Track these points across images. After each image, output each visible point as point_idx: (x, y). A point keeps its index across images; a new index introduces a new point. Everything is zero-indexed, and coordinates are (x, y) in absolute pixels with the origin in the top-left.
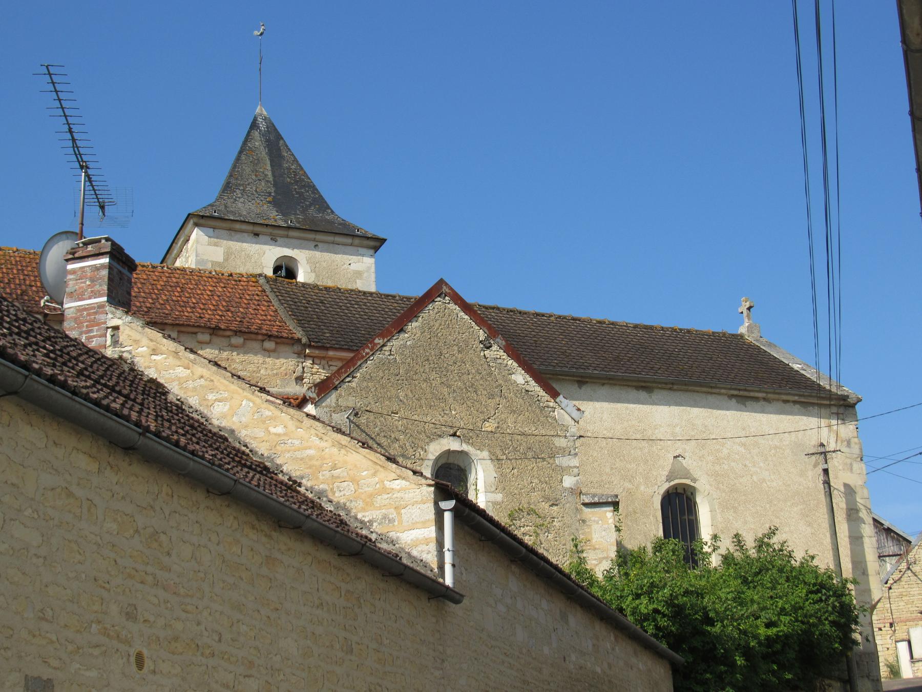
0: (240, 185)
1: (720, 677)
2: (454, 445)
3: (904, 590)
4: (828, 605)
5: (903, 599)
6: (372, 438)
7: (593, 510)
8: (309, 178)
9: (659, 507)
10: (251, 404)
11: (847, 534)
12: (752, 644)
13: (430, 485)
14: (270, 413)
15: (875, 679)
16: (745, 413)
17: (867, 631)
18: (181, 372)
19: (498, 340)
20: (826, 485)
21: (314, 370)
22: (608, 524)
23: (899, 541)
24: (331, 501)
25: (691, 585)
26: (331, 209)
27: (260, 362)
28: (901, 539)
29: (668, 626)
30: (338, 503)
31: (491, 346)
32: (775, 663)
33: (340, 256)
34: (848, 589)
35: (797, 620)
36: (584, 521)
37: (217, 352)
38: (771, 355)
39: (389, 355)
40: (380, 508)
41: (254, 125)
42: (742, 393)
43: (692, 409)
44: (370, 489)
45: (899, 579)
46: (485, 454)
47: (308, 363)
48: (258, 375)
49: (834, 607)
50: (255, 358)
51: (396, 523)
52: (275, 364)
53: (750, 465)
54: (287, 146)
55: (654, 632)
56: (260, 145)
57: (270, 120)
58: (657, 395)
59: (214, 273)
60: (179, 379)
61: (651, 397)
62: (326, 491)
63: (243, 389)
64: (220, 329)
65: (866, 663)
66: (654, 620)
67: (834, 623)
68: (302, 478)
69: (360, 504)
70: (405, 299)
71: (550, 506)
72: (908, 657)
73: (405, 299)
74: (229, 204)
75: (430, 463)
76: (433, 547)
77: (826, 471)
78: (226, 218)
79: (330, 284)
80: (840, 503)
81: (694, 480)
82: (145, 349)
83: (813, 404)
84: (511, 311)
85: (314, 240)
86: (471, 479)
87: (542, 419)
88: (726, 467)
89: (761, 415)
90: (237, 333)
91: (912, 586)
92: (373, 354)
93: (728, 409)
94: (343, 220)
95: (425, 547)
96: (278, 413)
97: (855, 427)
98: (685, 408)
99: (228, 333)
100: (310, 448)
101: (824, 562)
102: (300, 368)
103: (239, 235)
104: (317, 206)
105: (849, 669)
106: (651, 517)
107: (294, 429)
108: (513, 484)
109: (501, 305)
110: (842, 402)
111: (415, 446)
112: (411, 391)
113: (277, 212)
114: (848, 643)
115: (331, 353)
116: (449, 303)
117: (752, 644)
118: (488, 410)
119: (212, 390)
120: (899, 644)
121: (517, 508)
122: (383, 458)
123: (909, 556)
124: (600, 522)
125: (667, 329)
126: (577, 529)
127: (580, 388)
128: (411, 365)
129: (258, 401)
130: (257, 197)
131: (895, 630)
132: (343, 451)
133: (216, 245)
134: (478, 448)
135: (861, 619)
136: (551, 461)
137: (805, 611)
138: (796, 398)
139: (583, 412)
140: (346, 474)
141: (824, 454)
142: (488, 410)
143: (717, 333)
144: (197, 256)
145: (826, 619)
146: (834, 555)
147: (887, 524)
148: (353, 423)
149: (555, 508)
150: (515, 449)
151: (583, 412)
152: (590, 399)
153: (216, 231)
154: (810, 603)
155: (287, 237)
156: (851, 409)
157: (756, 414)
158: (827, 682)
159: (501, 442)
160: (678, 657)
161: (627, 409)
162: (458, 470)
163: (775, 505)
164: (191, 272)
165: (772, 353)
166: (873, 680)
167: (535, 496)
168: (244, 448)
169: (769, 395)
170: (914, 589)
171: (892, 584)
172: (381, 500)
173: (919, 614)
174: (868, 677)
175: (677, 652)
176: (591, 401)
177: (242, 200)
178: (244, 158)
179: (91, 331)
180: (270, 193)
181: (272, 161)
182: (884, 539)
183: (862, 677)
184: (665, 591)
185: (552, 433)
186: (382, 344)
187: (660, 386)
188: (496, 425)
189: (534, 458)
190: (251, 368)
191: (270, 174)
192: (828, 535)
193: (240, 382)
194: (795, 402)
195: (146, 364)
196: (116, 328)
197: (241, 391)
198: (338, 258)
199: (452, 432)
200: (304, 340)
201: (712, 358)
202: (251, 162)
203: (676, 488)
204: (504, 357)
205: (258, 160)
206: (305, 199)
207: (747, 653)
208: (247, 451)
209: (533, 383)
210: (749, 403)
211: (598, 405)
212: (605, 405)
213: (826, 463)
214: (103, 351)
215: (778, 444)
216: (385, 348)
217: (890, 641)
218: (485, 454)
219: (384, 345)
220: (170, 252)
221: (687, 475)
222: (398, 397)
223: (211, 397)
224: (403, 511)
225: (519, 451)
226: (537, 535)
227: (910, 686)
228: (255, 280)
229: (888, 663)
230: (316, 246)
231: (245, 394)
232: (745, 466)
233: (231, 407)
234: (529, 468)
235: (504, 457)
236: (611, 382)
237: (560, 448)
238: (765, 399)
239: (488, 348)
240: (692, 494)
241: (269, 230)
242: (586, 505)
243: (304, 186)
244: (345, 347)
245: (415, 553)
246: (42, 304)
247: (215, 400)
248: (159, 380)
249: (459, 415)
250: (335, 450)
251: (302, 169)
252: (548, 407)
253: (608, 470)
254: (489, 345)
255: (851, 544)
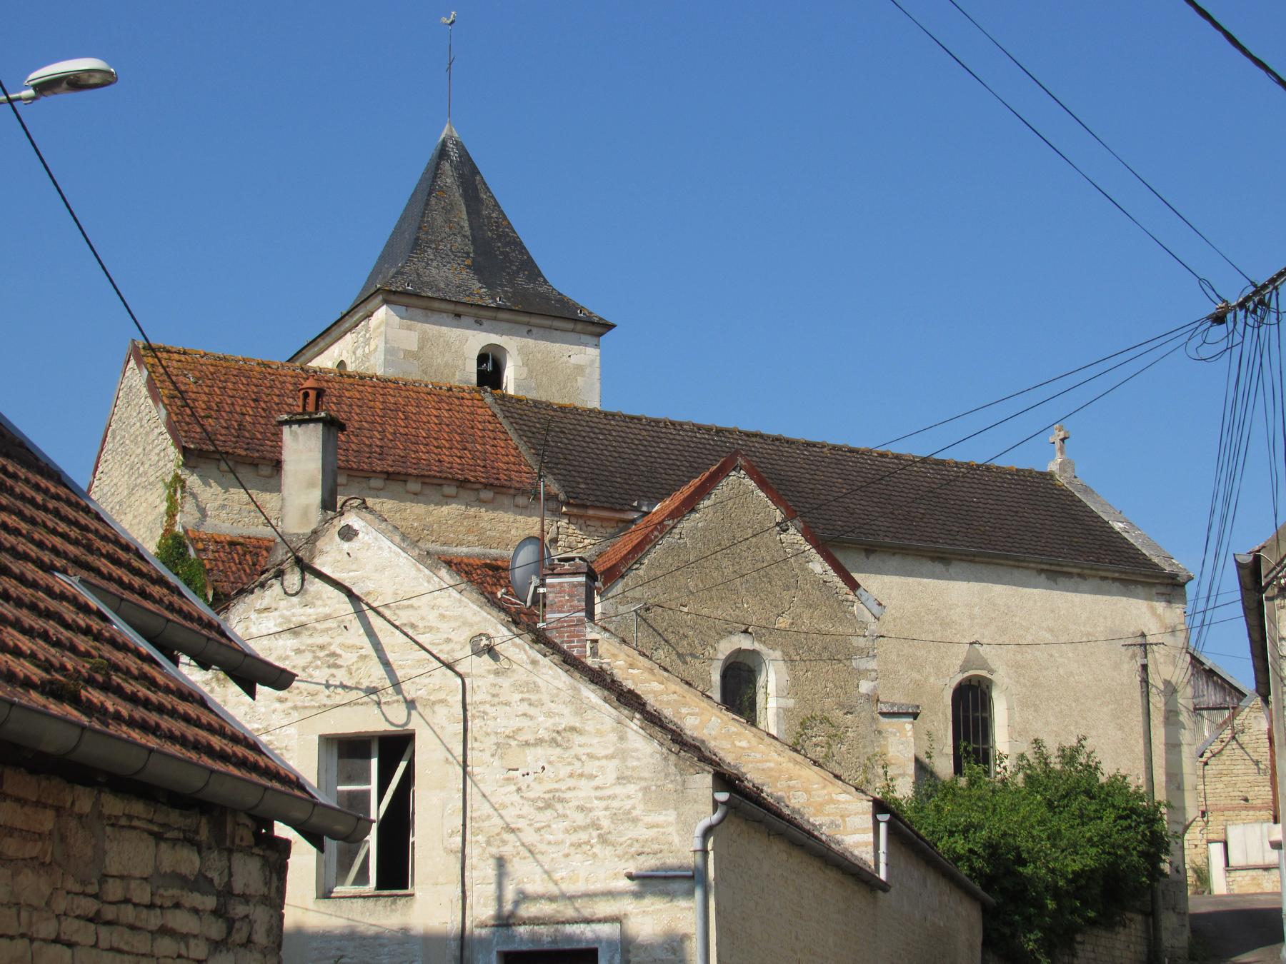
0: (431, 241)
1: (1028, 919)
2: (746, 643)
3: (1225, 767)
4: (1138, 833)
5: (1223, 779)
6: (660, 634)
7: (890, 720)
8: (515, 233)
9: (950, 702)
10: (719, 721)
11: (1163, 740)
12: (1060, 883)
13: (869, 801)
14: (735, 730)
15: (1182, 911)
16: (1055, 592)
17: (1177, 862)
18: (655, 686)
19: (796, 521)
20: (1144, 684)
21: (570, 531)
22: (907, 737)
23: (1224, 689)
24: (787, 806)
25: (1009, 828)
26: (543, 277)
27: (511, 520)
28: (1226, 686)
29: (983, 867)
30: (794, 808)
31: (788, 529)
32: (1078, 899)
33: (558, 345)
34: (1160, 812)
35: (1104, 852)
36: (880, 732)
37: (463, 507)
38: (1087, 506)
39: (679, 539)
40: (829, 815)
41: (443, 153)
42: (1053, 568)
43: (994, 585)
44: (820, 800)
45: (1220, 752)
46: (778, 654)
47: (563, 522)
48: (508, 536)
49: (1144, 835)
50: (505, 515)
51: (841, 828)
52: (526, 523)
53: (1057, 655)
54: (485, 184)
55: (968, 872)
56: (452, 184)
57: (463, 146)
58: (956, 568)
59: (431, 387)
60: (654, 692)
61: (947, 570)
62: (783, 797)
63: (712, 707)
64: (469, 481)
65: (1172, 893)
66: (969, 860)
67: (1142, 854)
68: (763, 785)
69: (812, 810)
70: (653, 424)
71: (845, 714)
72: (1222, 864)
73: (653, 424)
74: (421, 270)
75: (720, 663)
76: (871, 849)
77: (1145, 667)
78: (423, 294)
79: (566, 402)
80: (1157, 702)
81: (992, 671)
82: (622, 662)
83: (1136, 582)
84: (777, 440)
85: (528, 324)
86: (761, 680)
87: (840, 615)
88: (1029, 657)
89: (1074, 594)
90: (487, 486)
91: (1237, 762)
92: (662, 537)
93: (1035, 587)
94: (560, 294)
95: (864, 849)
96: (742, 730)
97: (1183, 611)
98: (986, 584)
99: (478, 486)
100: (769, 761)
101: (1136, 780)
102: (554, 528)
103: (436, 316)
104: (526, 273)
105: (1154, 900)
106: (940, 715)
107: (756, 744)
108: (805, 688)
109: (764, 431)
110: (1170, 581)
111: (704, 644)
112: (702, 581)
113: (480, 282)
114: (1156, 873)
115: (591, 512)
116: (744, 478)
117: (1060, 883)
118: (782, 603)
119: (685, 705)
120: (1212, 846)
121: (809, 716)
122: (832, 776)
123: (1236, 722)
124: (898, 734)
125: (962, 464)
126: (872, 741)
127: (868, 558)
128: (703, 550)
129: (725, 718)
130: (453, 260)
131: (1208, 821)
132: (798, 767)
133: (409, 328)
134: (770, 646)
135: (1173, 846)
136: (847, 663)
137: (1112, 840)
138: (1116, 575)
139: (885, 607)
140: (800, 785)
141: (1144, 645)
142: (782, 603)
143: (1022, 470)
144: (386, 343)
145: (1135, 849)
146: (1147, 768)
147: (1209, 663)
148: (640, 616)
149: (849, 716)
150: (809, 649)
151: (885, 607)
152: (879, 571)
153: (410, 310)
154: (1118, 830)
155: (495, 319)
156: (1179, 589)
157: (1068, 593)
158: (1129, 915)
159: (795, 640)
160: (990, 899)
161: (920, 584)
162: (748, 671)
163: (1082, 704)
164: (405, 385)
165: (1088, 504)
166: (1179, 913)
167: (829, 702)
168: (714, 757)
169: (1086, 572)
170: (1239, 767)
171: (1209, 758)
172: (829, 808)
173: (1242, 802)
174: (1174, 909)
175: (987, 892)
176: (879, 574)
177: (435, 263)
178: (433, 203)
179: (573, 642)
180: (468, 253)
181: (467, 206)
182: (1203, 685)
183: (1167, 909)
184: (983, 833)
185: (850, 631)
186: (672, 525)
187: (960, 557)
188: (790, 621)
189: (829, 659)
190: (501, 527)
191: (466, 224)
192: (1141, 742)
193: (709, 701)
194: (1114, 580)
195: (624, 676)
196: (595, 641)
197: (710, 709)
198: (556, 348)
199: (743, 628)
200: (562, 497)
201: (1017, 512)
202: (443, 208)
203: (970, 681)
204: (801, 542)
205: (451, 204)
206: (511, 262)
207: (1056, 893)
208: (717, 759)
209: (831, 572)
210: (1061, 580)
211: (887, 579)
212: (896, 579)
213: (1146, 657)
214: (583, 660)
215: (1091, 630)
216: (674, 531)
217: (1200, 836)
218: (778, 654)
219: (674, 527)
220: (339, 323)
221: (984, 665)
222: (688, 588)
223: (684, 710)
224: (847, 819)
225: (814, 651)
226: (830, 746)
227: (1221, 908)
228: (480, 398)
229: (1194, 865)
230: (529, 331)
231: (714, 711)
232: (1051, 656)
233: (701, 720)
234: (824, 670)
235: (798, 658)
236: (904, 551)
237: (858, 649)
238: (1079, 575)
239: (785, 531)
240: (987, 687)
241: (474, 311)
242: (883, 714)
243: (508, 244)
244: (606, 505)
245: (856, 853)
246: (499, 596)
247: (688, 714)
248: (636, 691)
249: (752, 610)
250: (791, 765)
251: (505, 218)
252: (847, 601)
253: (894, 657)
254: (786, 528)
255: (1166, 753)
